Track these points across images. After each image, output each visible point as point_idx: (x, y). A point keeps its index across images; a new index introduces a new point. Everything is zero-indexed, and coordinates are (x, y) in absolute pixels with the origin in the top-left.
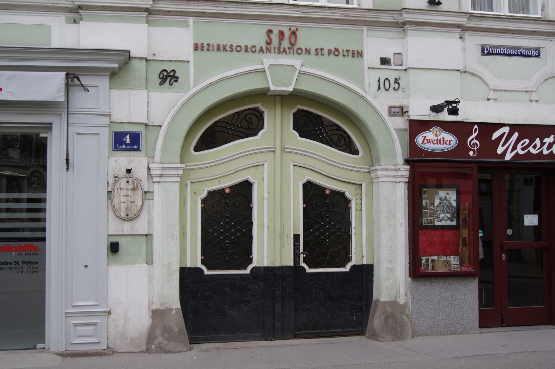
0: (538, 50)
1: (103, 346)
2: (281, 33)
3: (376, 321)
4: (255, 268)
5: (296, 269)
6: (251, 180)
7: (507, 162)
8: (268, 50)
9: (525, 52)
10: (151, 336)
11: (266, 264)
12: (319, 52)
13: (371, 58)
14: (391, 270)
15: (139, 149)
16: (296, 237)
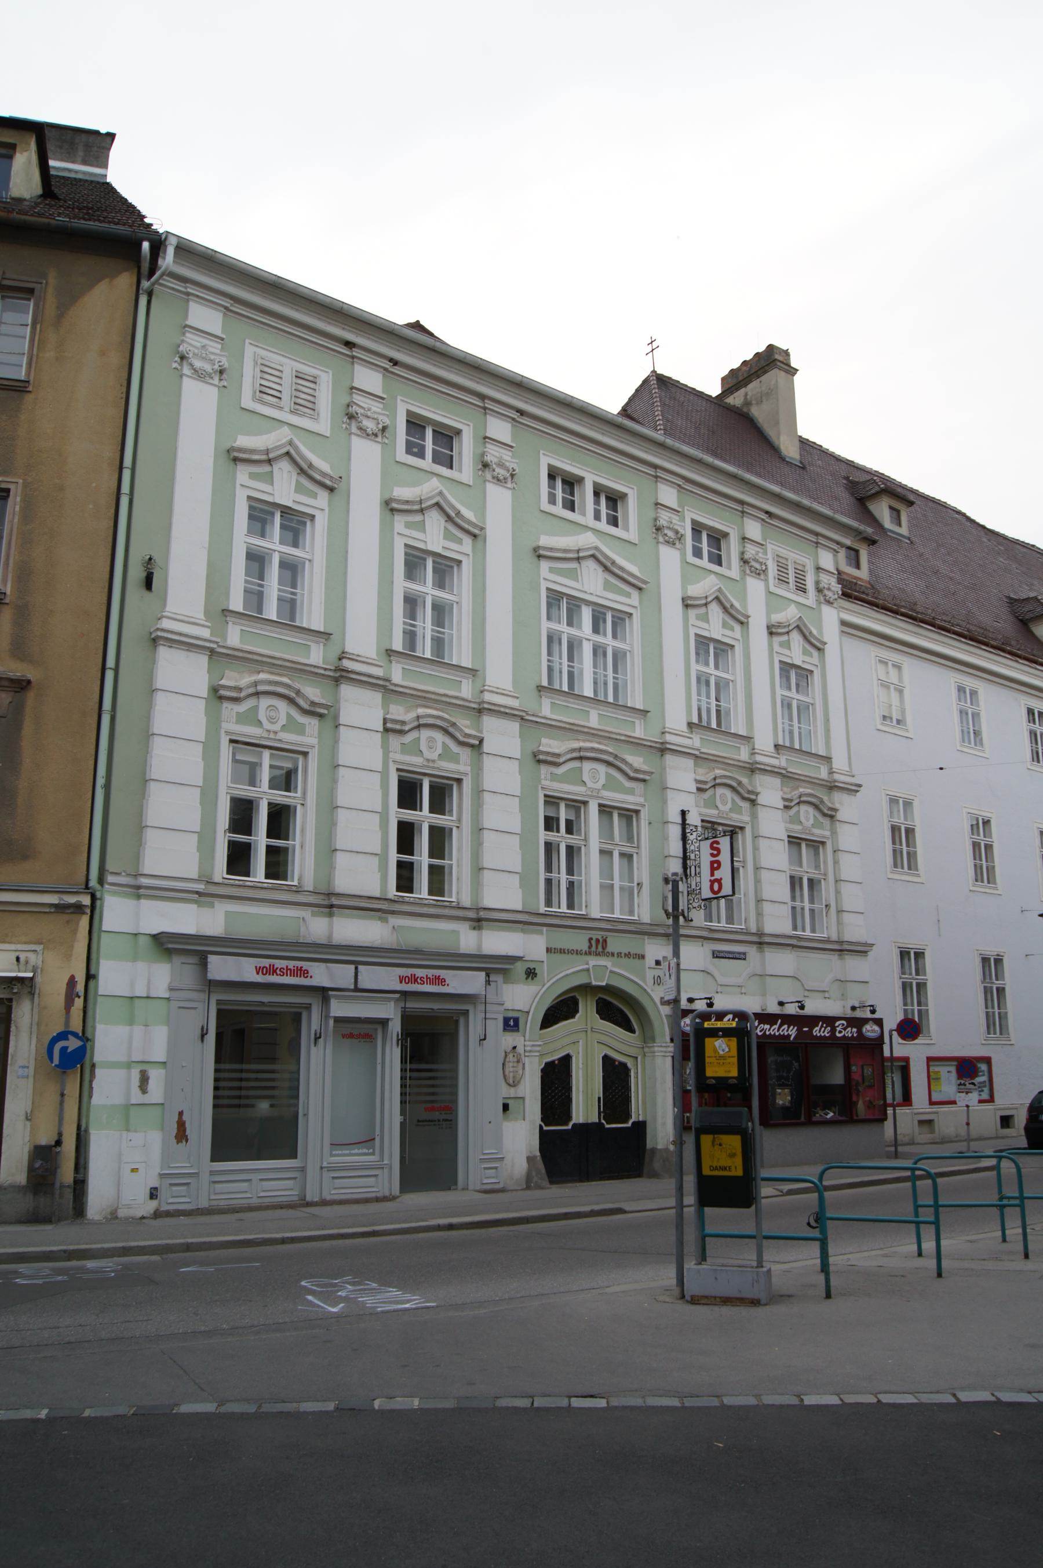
0: (744, 954)
1: (501, 1186)
2: (598, 941)
3: (657, 1165)
4: (574, 1125)
5: (599, 1125)
6: (572, 1053)
7: (792, 1043)
8: (590, 953)
9: (737, 956)
10: (529, 1178)
11: (581, 1121)
12: (619, 955)
13: (650, 961)
14: (664, 1124)
15: (518, 1030)
16: (599, 1099)
